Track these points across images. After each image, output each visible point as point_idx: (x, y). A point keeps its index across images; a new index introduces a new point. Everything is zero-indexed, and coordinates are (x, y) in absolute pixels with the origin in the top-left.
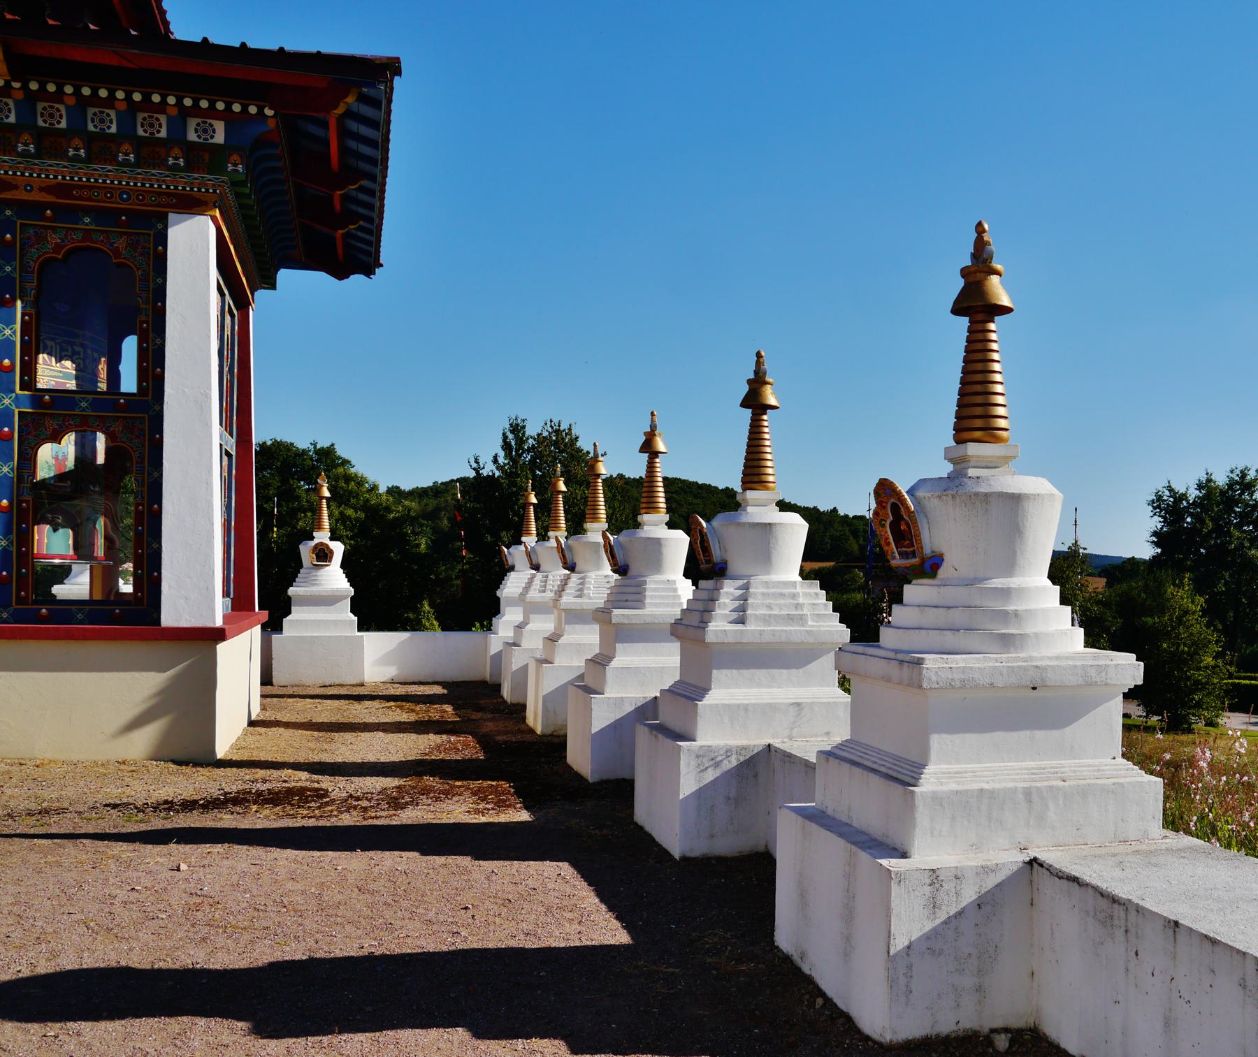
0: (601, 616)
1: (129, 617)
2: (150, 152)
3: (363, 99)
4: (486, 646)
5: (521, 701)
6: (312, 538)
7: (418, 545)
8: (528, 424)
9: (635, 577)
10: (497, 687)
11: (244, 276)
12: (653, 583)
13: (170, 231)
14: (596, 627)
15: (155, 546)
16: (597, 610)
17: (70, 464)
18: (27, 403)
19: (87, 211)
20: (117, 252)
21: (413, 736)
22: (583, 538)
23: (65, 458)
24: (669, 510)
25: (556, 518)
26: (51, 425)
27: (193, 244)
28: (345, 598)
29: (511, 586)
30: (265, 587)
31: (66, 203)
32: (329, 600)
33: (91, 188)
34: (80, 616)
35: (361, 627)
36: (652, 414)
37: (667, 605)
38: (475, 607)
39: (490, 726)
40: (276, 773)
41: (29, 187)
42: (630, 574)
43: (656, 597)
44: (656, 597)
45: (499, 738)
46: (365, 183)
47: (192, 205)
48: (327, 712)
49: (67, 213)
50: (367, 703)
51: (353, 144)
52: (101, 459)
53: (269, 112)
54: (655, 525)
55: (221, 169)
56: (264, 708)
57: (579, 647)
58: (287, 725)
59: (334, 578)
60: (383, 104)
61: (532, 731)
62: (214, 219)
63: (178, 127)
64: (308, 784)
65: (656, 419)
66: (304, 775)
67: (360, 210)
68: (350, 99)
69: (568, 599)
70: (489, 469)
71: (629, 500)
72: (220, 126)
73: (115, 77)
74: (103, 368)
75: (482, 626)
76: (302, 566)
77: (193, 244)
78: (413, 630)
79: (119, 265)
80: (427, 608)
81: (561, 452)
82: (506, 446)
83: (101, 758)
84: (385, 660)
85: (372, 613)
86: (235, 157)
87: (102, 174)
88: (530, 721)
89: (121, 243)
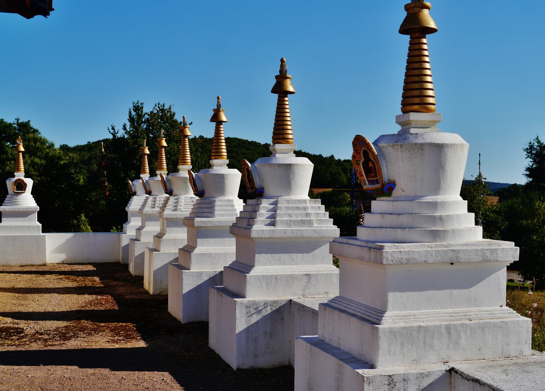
4: (119, 241)
6: (14, 176)
7: (79, 180)
12: (219, 202)
16: (186, 218)
21: (75, 296)
25: (161, 163)
28: (34, 212)
32: (24, 214)
36: (218, 98)
38: (113, 218)
39: (122, 290)
42: (205, 196)
43: (221, 210)
48: (23, 281)
54: (220, 166)
59: (28, 200)
61: (147, 293)
64: (11, 325)
65: (220, 101)
66: (9, 320)
69: (168, 212)
70: (121, 133)
75: (117, 229)
81: (164, 123)
82: (131, 119)
84: (60, 250)
85: (52, 219)
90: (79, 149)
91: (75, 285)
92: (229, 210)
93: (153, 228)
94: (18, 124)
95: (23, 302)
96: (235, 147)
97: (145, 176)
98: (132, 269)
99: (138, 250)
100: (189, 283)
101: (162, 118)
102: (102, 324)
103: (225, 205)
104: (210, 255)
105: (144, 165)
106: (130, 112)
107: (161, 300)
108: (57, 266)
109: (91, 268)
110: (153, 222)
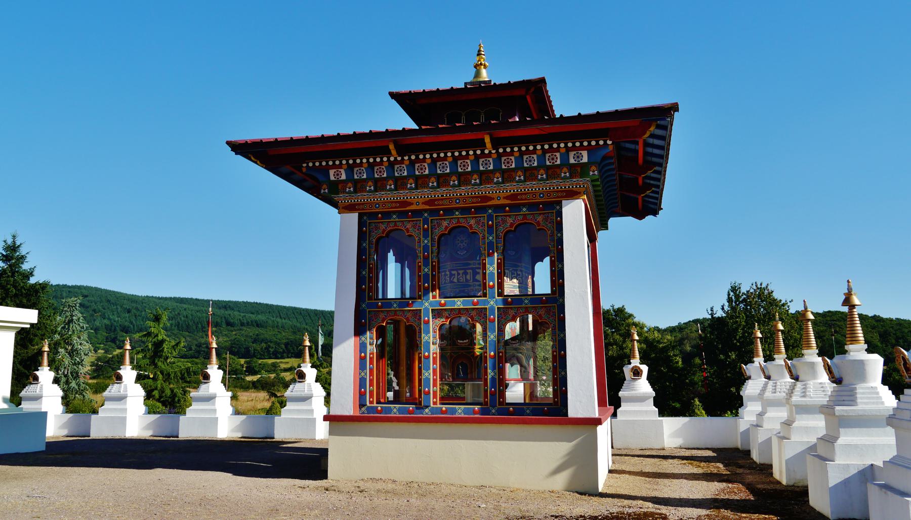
0: (827, 410)
1: (550, 410)
2: (553, 172)
3: (659, 127)
4: (736, 426)
5: (767, 462)
6: (630, 363)
7: (677, 363)
8: (742, 286)
9: (847, 386)
10: (748, 453)
11: (596, 223)
12: (861, 389)
13: (564, 210)
14: (822, 416)
15: (563, 373)
16: (823, 406)
17: (518, 332)
18: (501, 302)
19: (524, 205)
20: (471, 226)
21: (705, 483)
22: (802, 360)
23: (515, 329)
24: (866, 342)
25: (779, 347)
26: (512, 312)
27: (574, 213)
28: (649, 398)
29: (750, 389)
30: (611, 393)
31: (515, 204)
32: (641, 399)
33: (525, 194)
34: (528, 411)
35: (661, 414)
36: (848, 281)
37: (873, 403)
38: (725, 400)
39: (750, 478)
40: (634, 503)
41: (499, 198)
42: (844, 383)
43: (864, 398)
44: (864, 398)
45: (759, 486)
46: (657, 168)
47: (572, 195)
48: (650, 465)
49: (515, 208)
50: (671, 461)
51: (650, 150)
52: (531, 328)
53: (609, 142)
54: (857, 351)
55: (587, 175)
56: (613, 463)
57: (807, 430)
58: (630, 473)
59: (643, 386)
60: (667, 128)
61: (779, 483)
62: (584, 200)
63: (565, 158)
64: (653, 510)
65: (851, 284)
66: (650, 505)
67: (652, 182)
68: (652, 129)
69: (796, 398)
70: (719, 314)
71: (833, 333)
72: (585, 154)
73: (534, 139)
74: (530, 280)
75: (732, 413)
76: (625, 379)
77: (574, 213)
78: (690, 416)
79: (539, 230)
80: (697, 402)
81: (762, 301)
82: (730, 300)
83: (541, 489)
84: (676, 434)
85: (666, 405)
86: (593, 168)
87: (532, 186)
88: (777, 474)
89: (540, 218)
90: (671, 330)
91: (700, 471)
92: (873, 398)
93: (782, 414)
94: (614, 310)
95: (655, 487)
96: (838, 320)
97: (759, 360)
98: (755, 456)
99: (761, 436)
100: (835, 477)
101: (759, 296)
102: (744, 515)
103: (869, 393)
104: (856, 446)
105: (757, 348)
106: (729, 295)
107: (800, 493)
108: (676, 451)
109: (710, 453)
110: (856, 430)
